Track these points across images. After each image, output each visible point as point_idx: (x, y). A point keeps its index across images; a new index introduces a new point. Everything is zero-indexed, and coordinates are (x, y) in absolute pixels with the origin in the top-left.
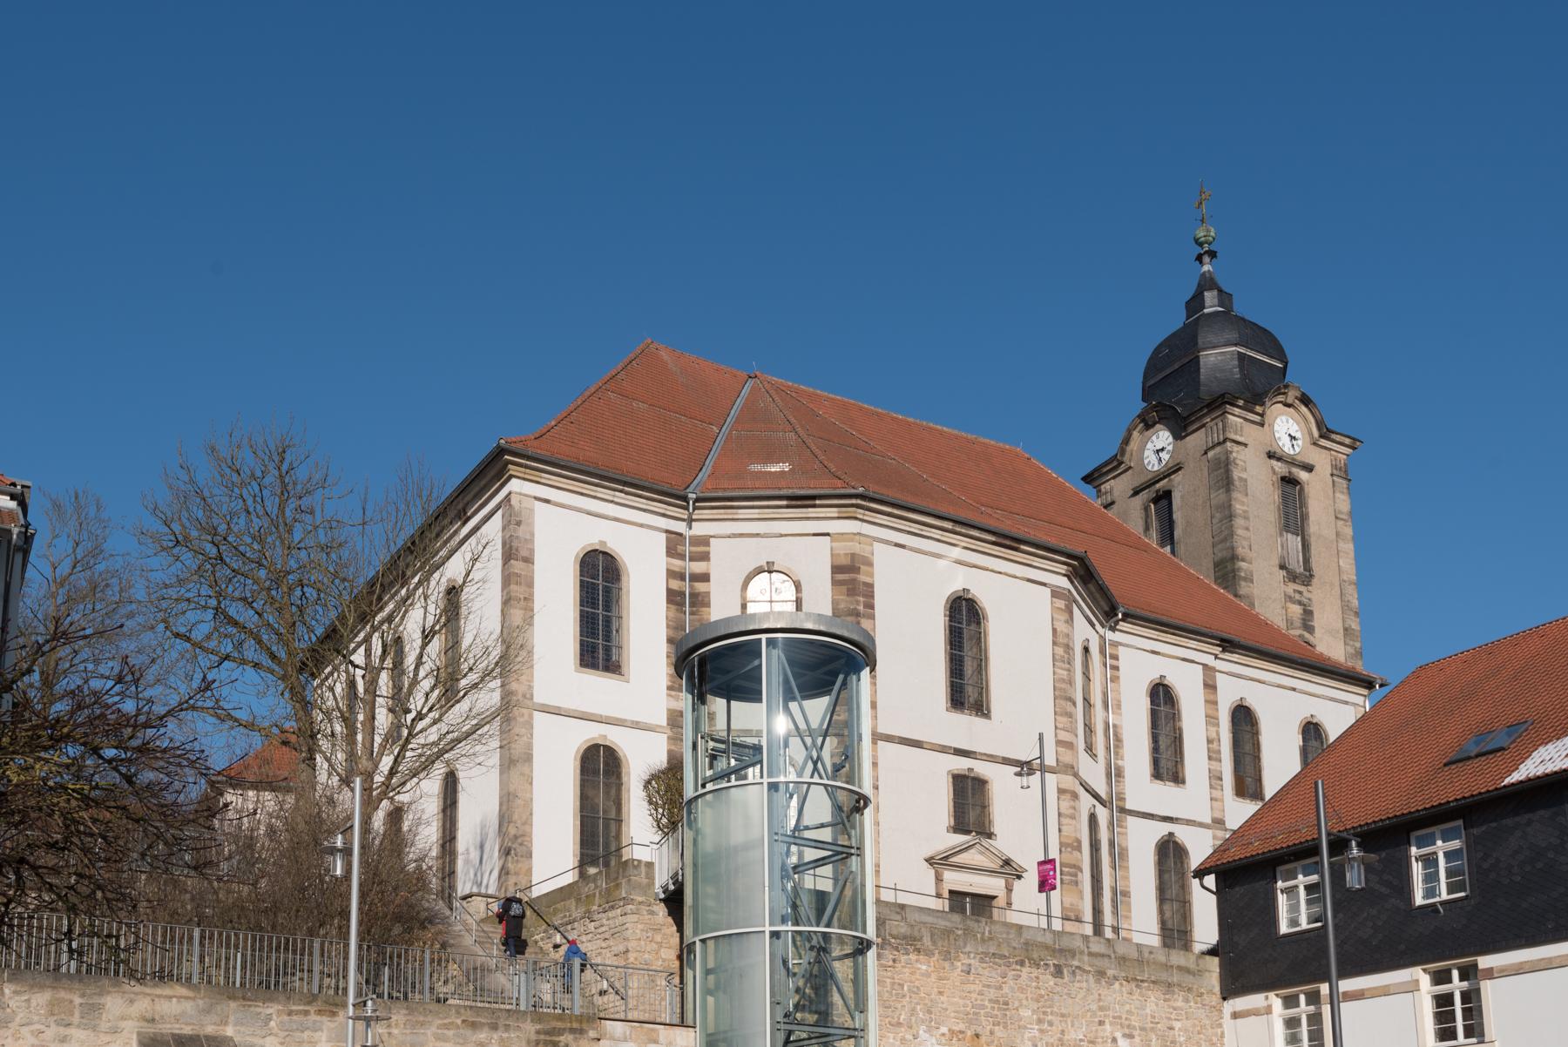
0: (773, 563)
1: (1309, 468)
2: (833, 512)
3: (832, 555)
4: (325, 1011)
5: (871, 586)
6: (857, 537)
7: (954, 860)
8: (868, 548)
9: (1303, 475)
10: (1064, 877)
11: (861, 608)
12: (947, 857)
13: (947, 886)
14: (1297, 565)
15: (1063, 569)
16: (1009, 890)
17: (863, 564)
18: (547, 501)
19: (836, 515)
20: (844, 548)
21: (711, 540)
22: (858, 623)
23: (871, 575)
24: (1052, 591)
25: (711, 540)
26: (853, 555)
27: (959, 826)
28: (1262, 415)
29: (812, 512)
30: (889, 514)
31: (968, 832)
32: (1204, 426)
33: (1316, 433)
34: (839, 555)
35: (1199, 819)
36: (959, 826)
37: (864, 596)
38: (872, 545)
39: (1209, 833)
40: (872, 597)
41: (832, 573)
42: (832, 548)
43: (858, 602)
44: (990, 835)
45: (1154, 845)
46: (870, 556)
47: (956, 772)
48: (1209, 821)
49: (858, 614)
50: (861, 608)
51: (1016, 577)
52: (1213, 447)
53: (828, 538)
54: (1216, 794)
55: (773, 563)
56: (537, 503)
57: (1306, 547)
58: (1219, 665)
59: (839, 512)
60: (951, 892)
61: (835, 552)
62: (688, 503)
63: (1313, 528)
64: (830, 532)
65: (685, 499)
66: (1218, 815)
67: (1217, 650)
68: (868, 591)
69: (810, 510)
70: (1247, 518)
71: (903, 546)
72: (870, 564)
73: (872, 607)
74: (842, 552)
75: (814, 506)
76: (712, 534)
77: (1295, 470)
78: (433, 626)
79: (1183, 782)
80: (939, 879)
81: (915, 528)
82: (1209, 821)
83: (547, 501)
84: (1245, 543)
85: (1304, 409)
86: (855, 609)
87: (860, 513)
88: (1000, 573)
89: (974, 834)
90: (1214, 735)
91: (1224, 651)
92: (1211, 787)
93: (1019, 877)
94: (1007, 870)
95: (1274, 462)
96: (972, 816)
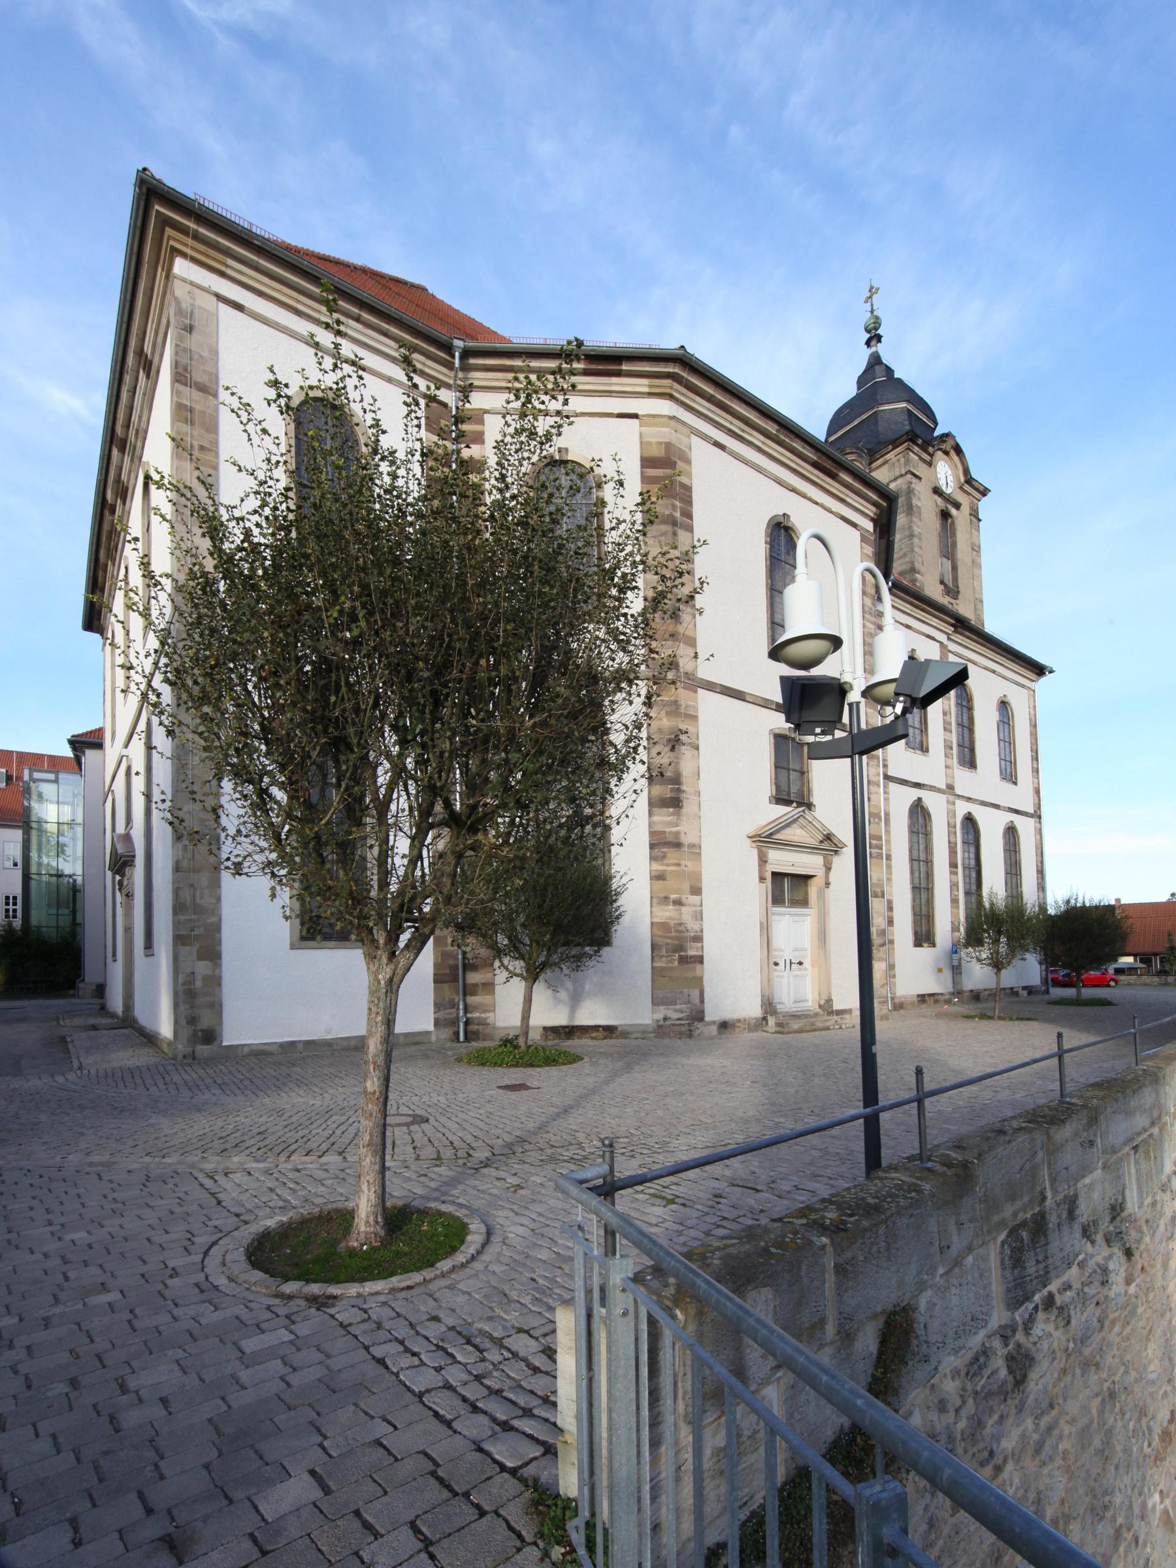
0: (567, 450)
1: (957, 506)
2: (642, 385)
3: (641, 443)
4: (977, 490)
5: (688, 489)
6: (672, 423)
7: (777, 836)
8: (685, 440)
9: (953, 511)
10: (873, 851)
11: (678, 515)
12: (771, 834)
13: (771, 868)
14: (949, 580)
15: (871, 510)
16: (828, 868)
17: (680, 459)
18: (239, 307)
19: (646, 390)
20: (661, 434)
21: (486, 416)
22: (675, 534)
23: (690, 476)
24: (862, 535)
25: (486, 416)
26: (668, 445)
27: (781, 799)
28: (932, 455)
29: (616, 383)
30: (710, 399)
31: (788, 803)
32: (886, 462)
33: (962, 479)
34: (650, 443)
35: (938, 786)
36: (781, 799)
37: (681, 500)
38: (689, 437)
39: (944, 797)
40: (690, 503)
41: (643, 466)
42: (641, 434)
43: (674, 507)
44: (810, 806)
45: (931, 811)
46: (686, 450)
47: (777, 731)
48: (944, 787)
49: (674, 523)
50: (678, 515)
51: (831, 512)
52: (896, 479)
53: (636, 421)
54: (949, 761)
55: (567, 450)
56: (224, 309)
57: (954, 568)
58: (952, 646)
59: (650, 386)
60: (774, 874)
61: (646, 439)
62: (453, 357)
63: (959, 555)
64: (640, 413)
65: (448, 349)
66: (950, 782)
67: (950, 629)
68: (685, 495)
69: (614, 380)
70: (920, 539)
71: (721, 447)
72: (688, 461)
73: (690, 516)
74: (654, 440)
75: (619, 374)
76: (487, 407)
77: (949, 507)
78: (449, 681)
79: (927, 751)
80: (763, 860)
81: (736, 426)
82: (944, 787)
83: (239, 307)
84: (920, 559)
85: (956, 458)
86: (671, 515)
87: (678, 390)
88: (817, 503)
89: (795, 804)
90: (947, 708)
91: (955, 631)
92: (946, 756)
93: (836, 852)
94: (826, 845)
95: (936, 497)
96: (96, 623)
